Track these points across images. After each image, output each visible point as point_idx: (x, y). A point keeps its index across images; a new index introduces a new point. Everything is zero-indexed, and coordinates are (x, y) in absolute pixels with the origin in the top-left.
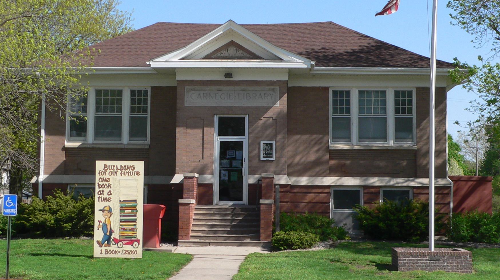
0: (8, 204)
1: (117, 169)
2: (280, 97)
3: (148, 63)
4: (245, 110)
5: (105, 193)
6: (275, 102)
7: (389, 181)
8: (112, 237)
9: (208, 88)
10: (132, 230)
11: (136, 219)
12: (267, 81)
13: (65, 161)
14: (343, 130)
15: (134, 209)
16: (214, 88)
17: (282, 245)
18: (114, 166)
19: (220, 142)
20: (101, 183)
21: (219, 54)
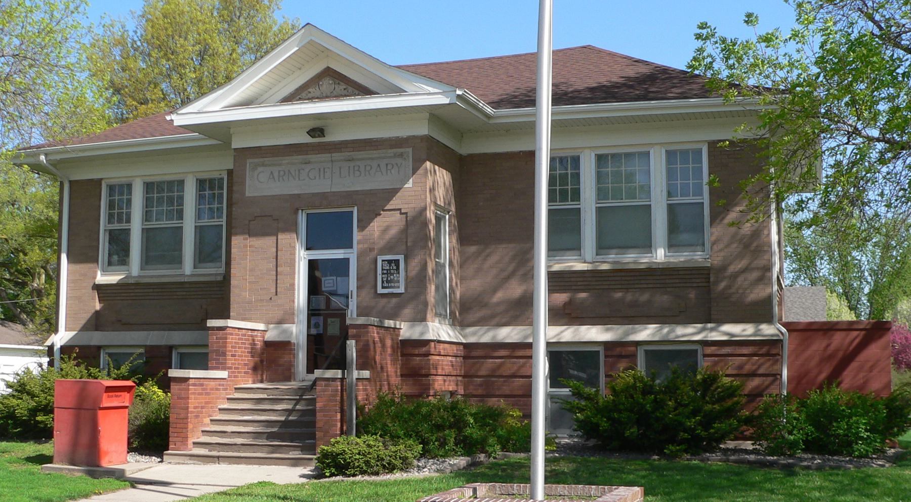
3: (168, 118)
4: (350, 197)
9: (286, 160)
19: (310, 261)
21: (304, 95)
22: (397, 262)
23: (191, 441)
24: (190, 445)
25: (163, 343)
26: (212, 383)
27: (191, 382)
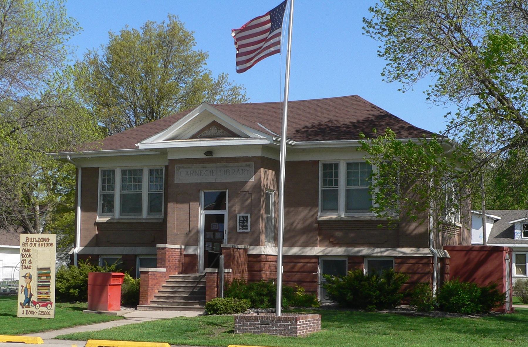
1: (36, 241)
3: (136, 145)
5: (27, 262)
8: (32, 300)
10: (47, 293)
11: (50, 285)
12: (243, 157)
13: (97, 235)
14: (331, 202)
15: (48, 276)
20: (24, 253)
21: (202, 134)
22: (247, 217)
23: (149, 300)
24: (149, 302)
25: (131, 253)
26: (159, 274)
27: (150, 273)
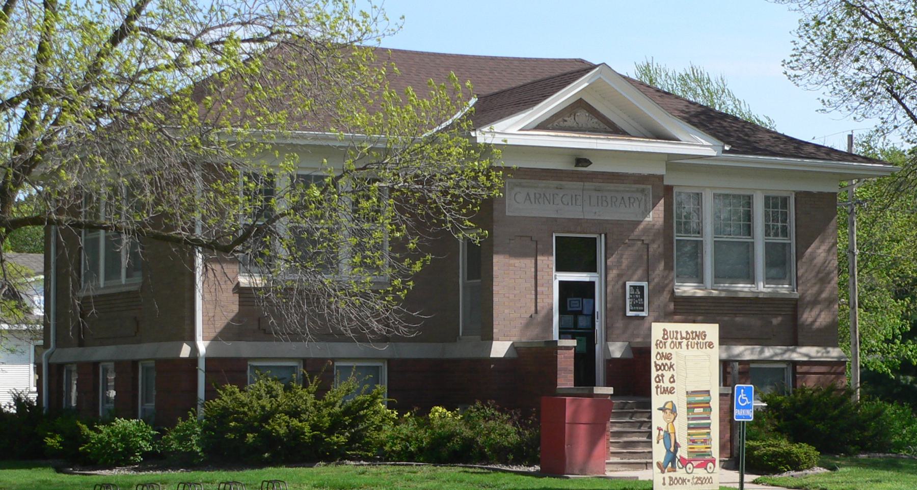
0: (743, 401)
1: (682, 338)
2: (654, 205)
5: (666, 379)
6: (646, 213)
7: (762, 352)
8: (678, 455)
9: (543, 183)
10: (705, 442)
12: (633, 175)
16: (554, 183)
17: (780, 463)
18: (677, 332)
20: (659, 362)
22: (642, 288)
